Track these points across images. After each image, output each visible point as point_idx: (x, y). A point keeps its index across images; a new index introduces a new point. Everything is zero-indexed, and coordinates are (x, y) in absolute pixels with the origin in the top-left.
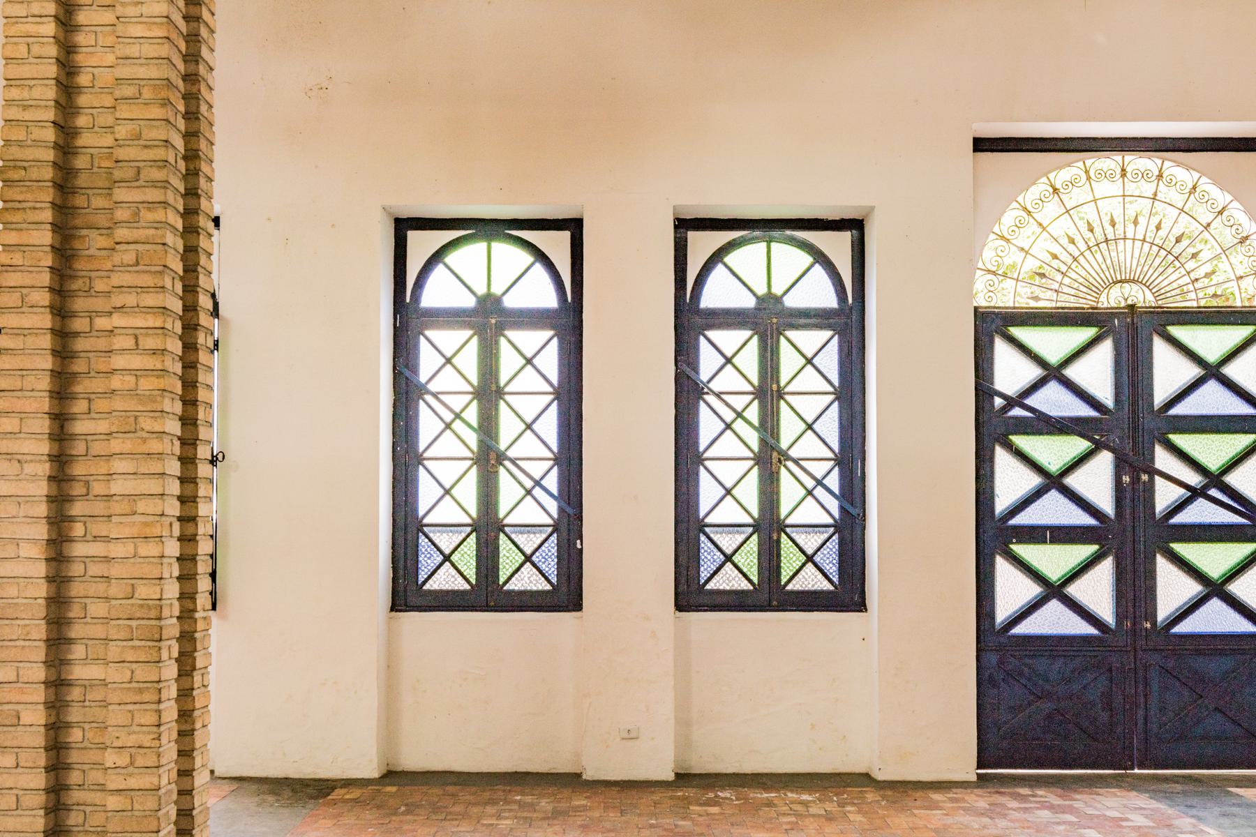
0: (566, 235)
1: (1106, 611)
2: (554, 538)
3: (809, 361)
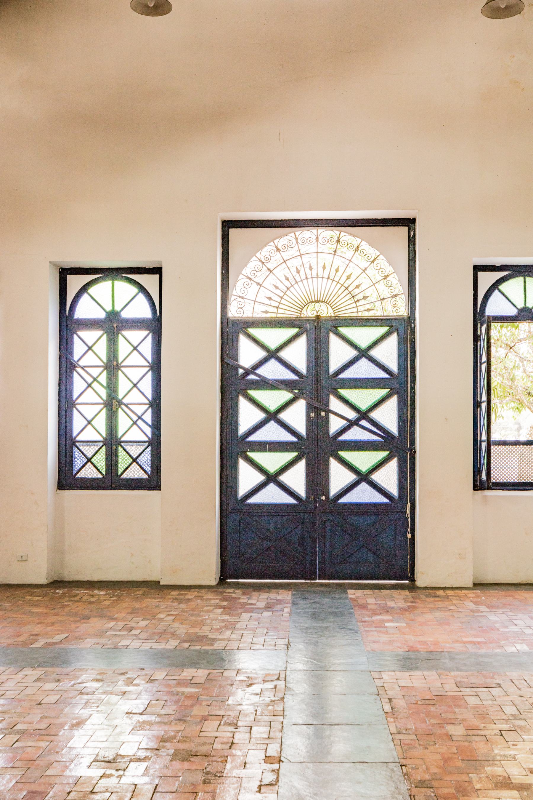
0: (69, 277)
1: (301, 490)
2: (149, 449)
3: (90, 348)
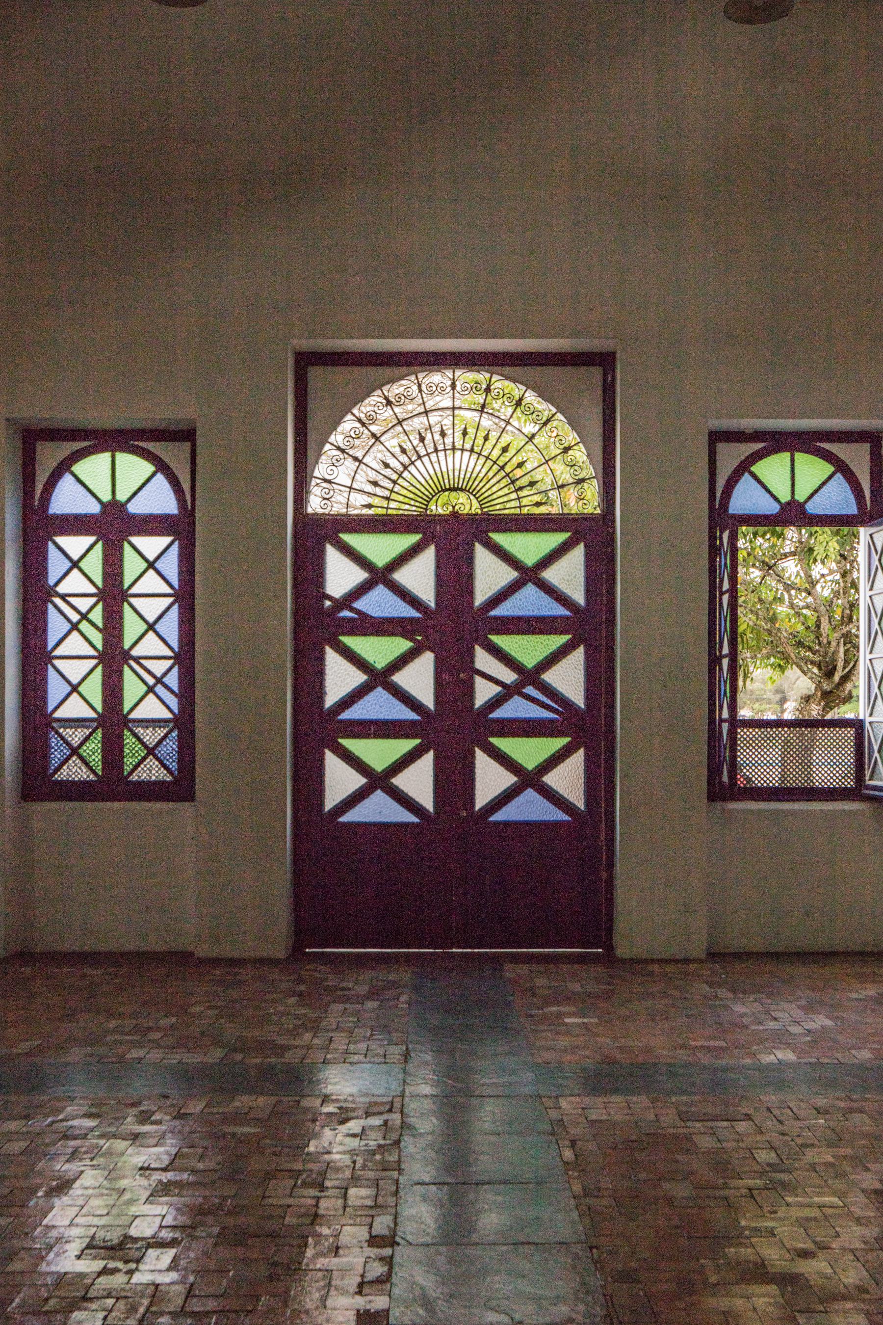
1: (426, 799)
